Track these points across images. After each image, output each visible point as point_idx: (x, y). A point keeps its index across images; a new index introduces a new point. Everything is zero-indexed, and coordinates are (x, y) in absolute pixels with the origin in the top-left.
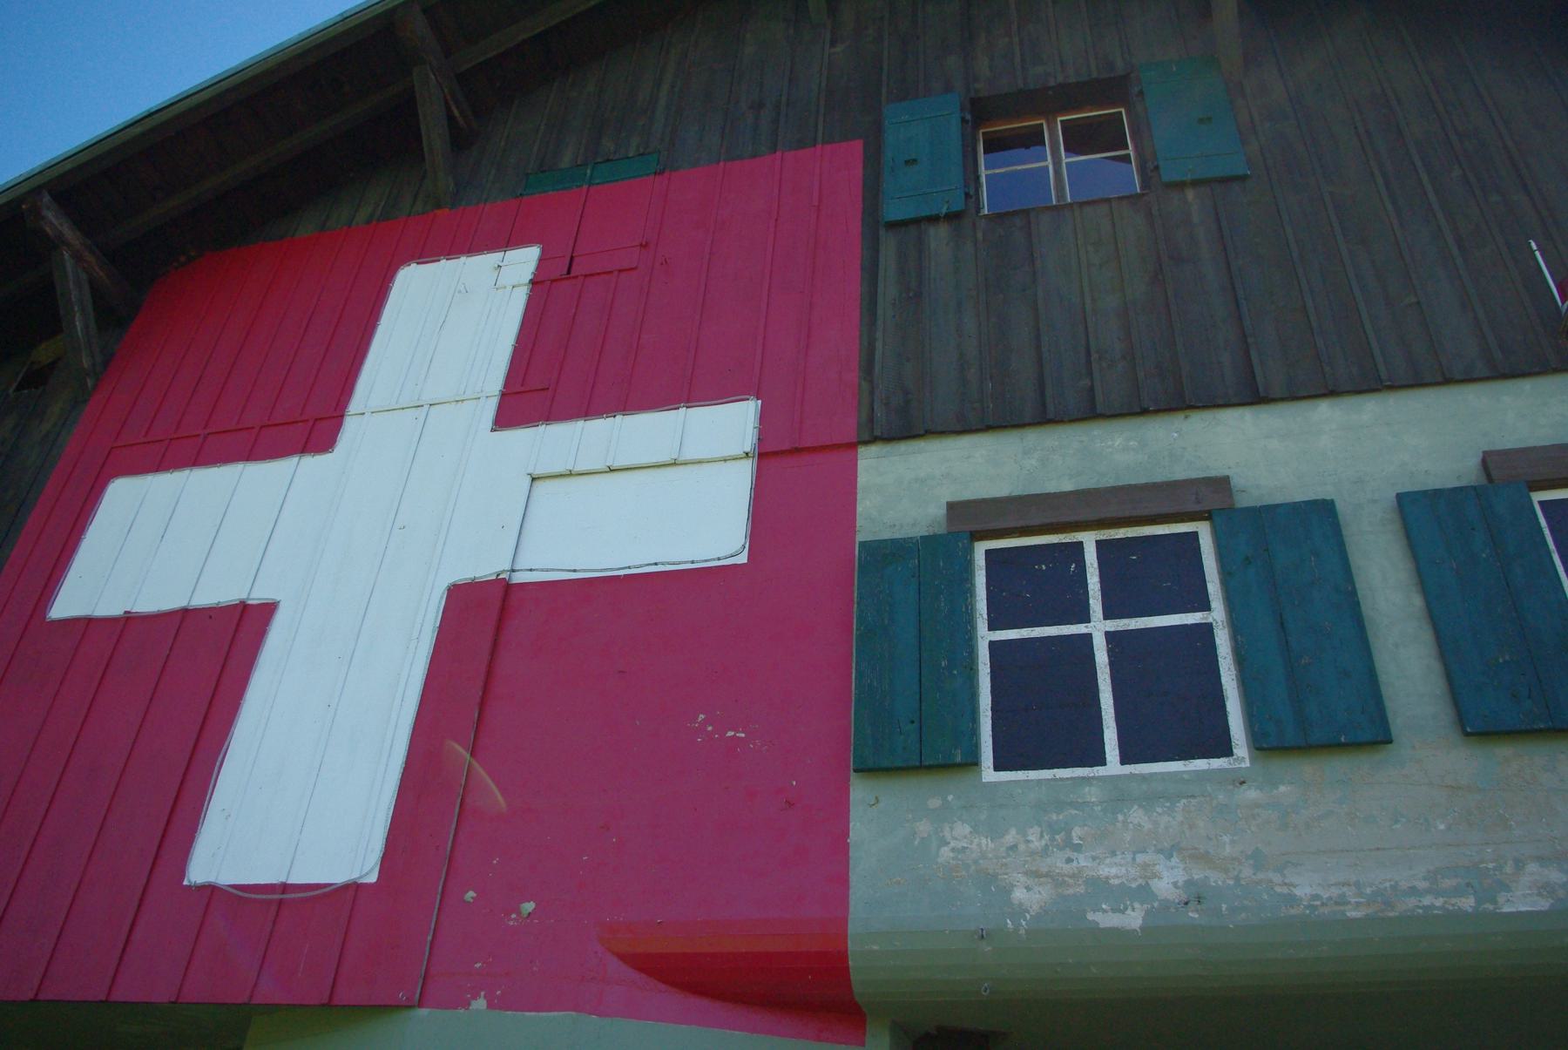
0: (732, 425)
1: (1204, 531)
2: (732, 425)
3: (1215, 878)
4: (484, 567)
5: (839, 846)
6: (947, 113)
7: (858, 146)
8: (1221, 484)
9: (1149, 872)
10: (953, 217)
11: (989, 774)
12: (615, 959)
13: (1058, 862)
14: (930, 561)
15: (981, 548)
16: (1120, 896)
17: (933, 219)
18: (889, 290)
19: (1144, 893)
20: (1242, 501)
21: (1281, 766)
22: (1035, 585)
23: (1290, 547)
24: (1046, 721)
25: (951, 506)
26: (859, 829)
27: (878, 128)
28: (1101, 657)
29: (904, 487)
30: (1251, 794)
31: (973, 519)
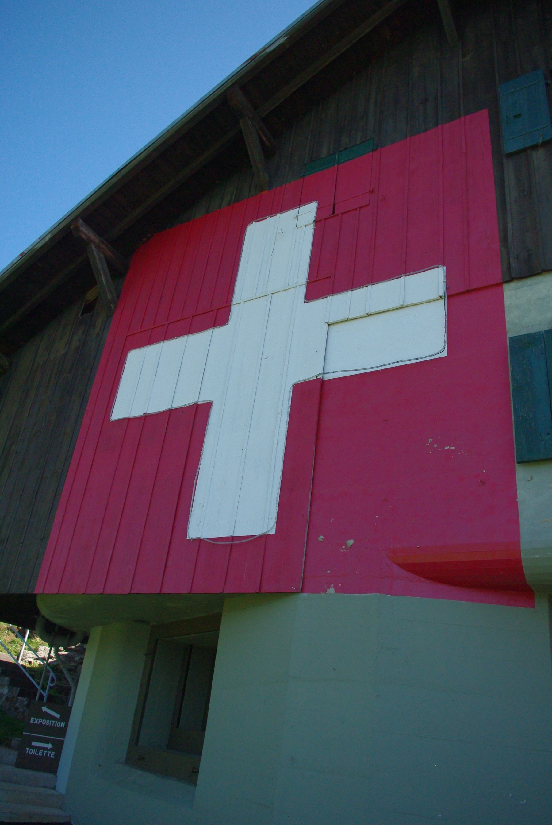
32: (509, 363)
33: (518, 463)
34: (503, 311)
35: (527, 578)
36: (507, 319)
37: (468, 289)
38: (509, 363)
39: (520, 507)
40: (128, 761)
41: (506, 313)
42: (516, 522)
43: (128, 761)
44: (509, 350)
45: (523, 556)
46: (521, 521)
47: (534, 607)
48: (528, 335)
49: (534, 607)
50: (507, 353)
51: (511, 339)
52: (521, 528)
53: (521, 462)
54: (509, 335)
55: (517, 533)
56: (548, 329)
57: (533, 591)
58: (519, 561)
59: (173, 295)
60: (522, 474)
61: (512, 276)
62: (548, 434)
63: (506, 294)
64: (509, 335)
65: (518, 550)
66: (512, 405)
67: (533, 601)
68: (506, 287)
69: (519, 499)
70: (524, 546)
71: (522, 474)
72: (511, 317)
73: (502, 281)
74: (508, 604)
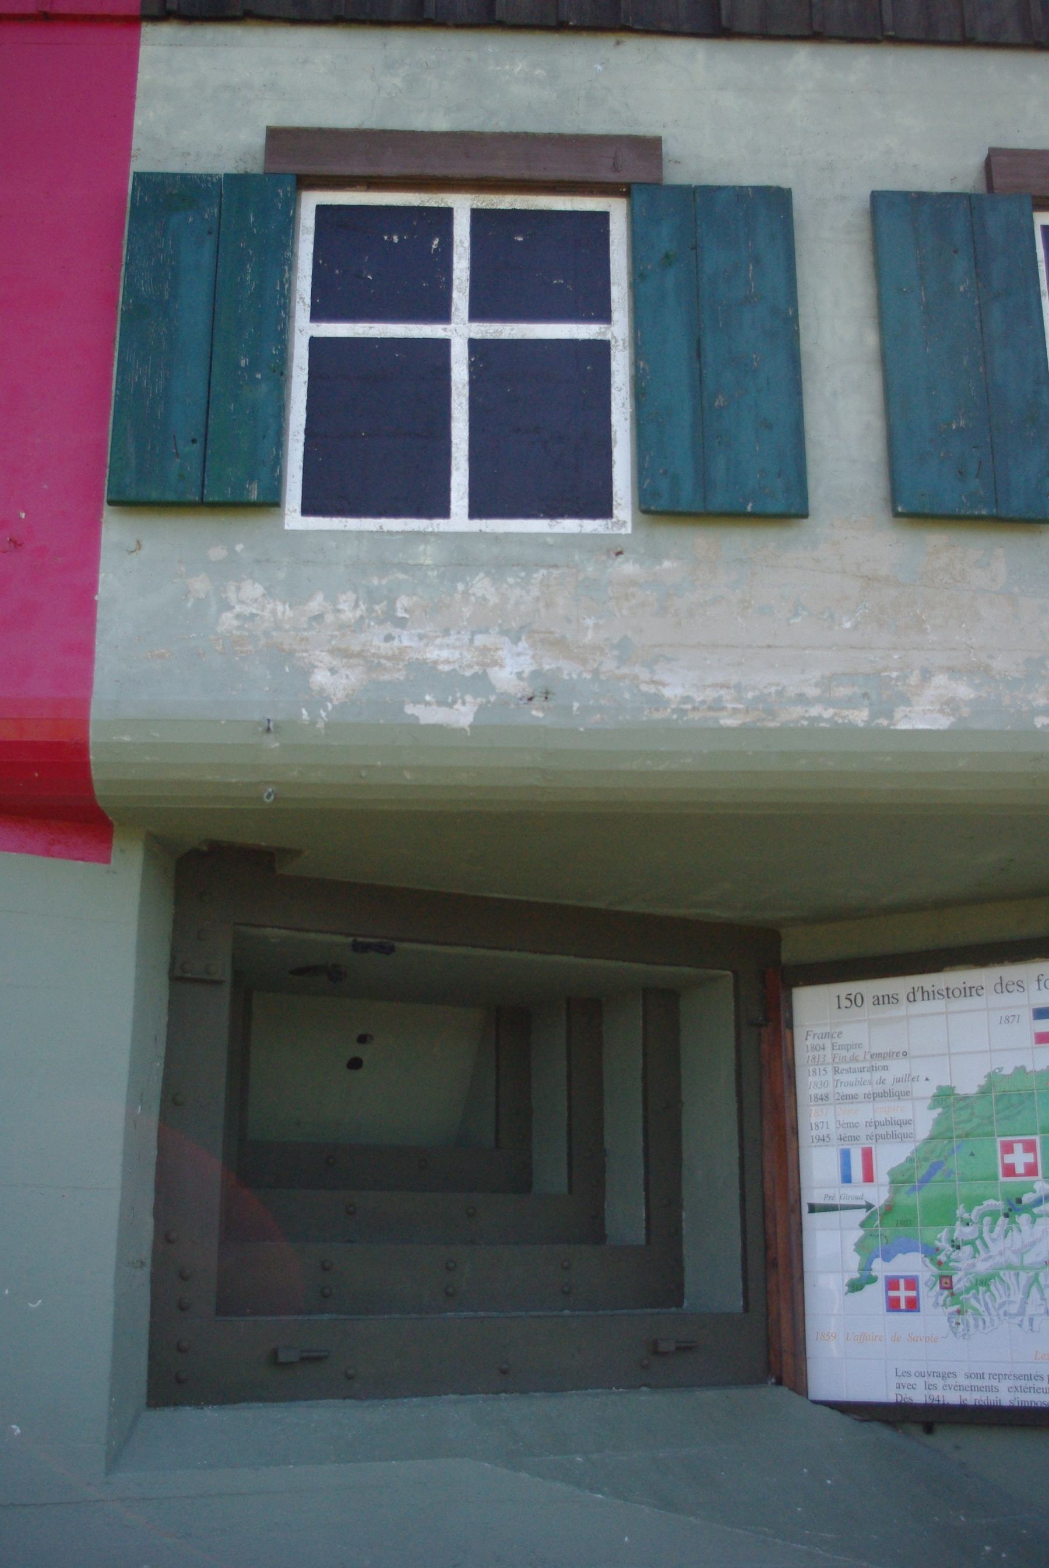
3: (570, 670)
8: (649, 147)
9: (488, 658)
11: (293, 517)
13: (375, 640)
15: (310, 201)
16: (448, 686)
19: (480, 683)
20: (675, 175)
23: (724, 243)
24: (376, 456)
25: (276, 136)
30: (627, 568)
31: (302, 155)
32: (125, 242)
33: (111, 503)
34: (132, 97)
35: (99, 790)
36: (138, 122)
37: (47, 9)
38: (125, 242)
39: (101, 614)
40: (888, 1310)
41: (139, 103)
42: (85, 650)
43: (888, 1310)
44: (129, 205)
45: (94, 737)
46: (101, 648)
47: (107, 861)
48: (185, 177)
49: (107, 861)
50: (123, 212)
51: (138, 176)
52: (97, 666)
53: (124, 503)
54: (136, 166)
55: (84, 677)
56: (234, 172)
57: (110, 825)
58: (81, 749)
59: (933, 1056)
60: (116, 530)
61: (169, 6)
62: (194, 441)
63: (146, 52)
64: (136, 166)
65: (83, 723)
66: (116, 354)
67: (110, 848)
68: (148, 31)
69: (102, 594)
70: (97, 713)
71: (116, 530)
72: (147, 117)
73: (138, 13)
74: (47, 853)
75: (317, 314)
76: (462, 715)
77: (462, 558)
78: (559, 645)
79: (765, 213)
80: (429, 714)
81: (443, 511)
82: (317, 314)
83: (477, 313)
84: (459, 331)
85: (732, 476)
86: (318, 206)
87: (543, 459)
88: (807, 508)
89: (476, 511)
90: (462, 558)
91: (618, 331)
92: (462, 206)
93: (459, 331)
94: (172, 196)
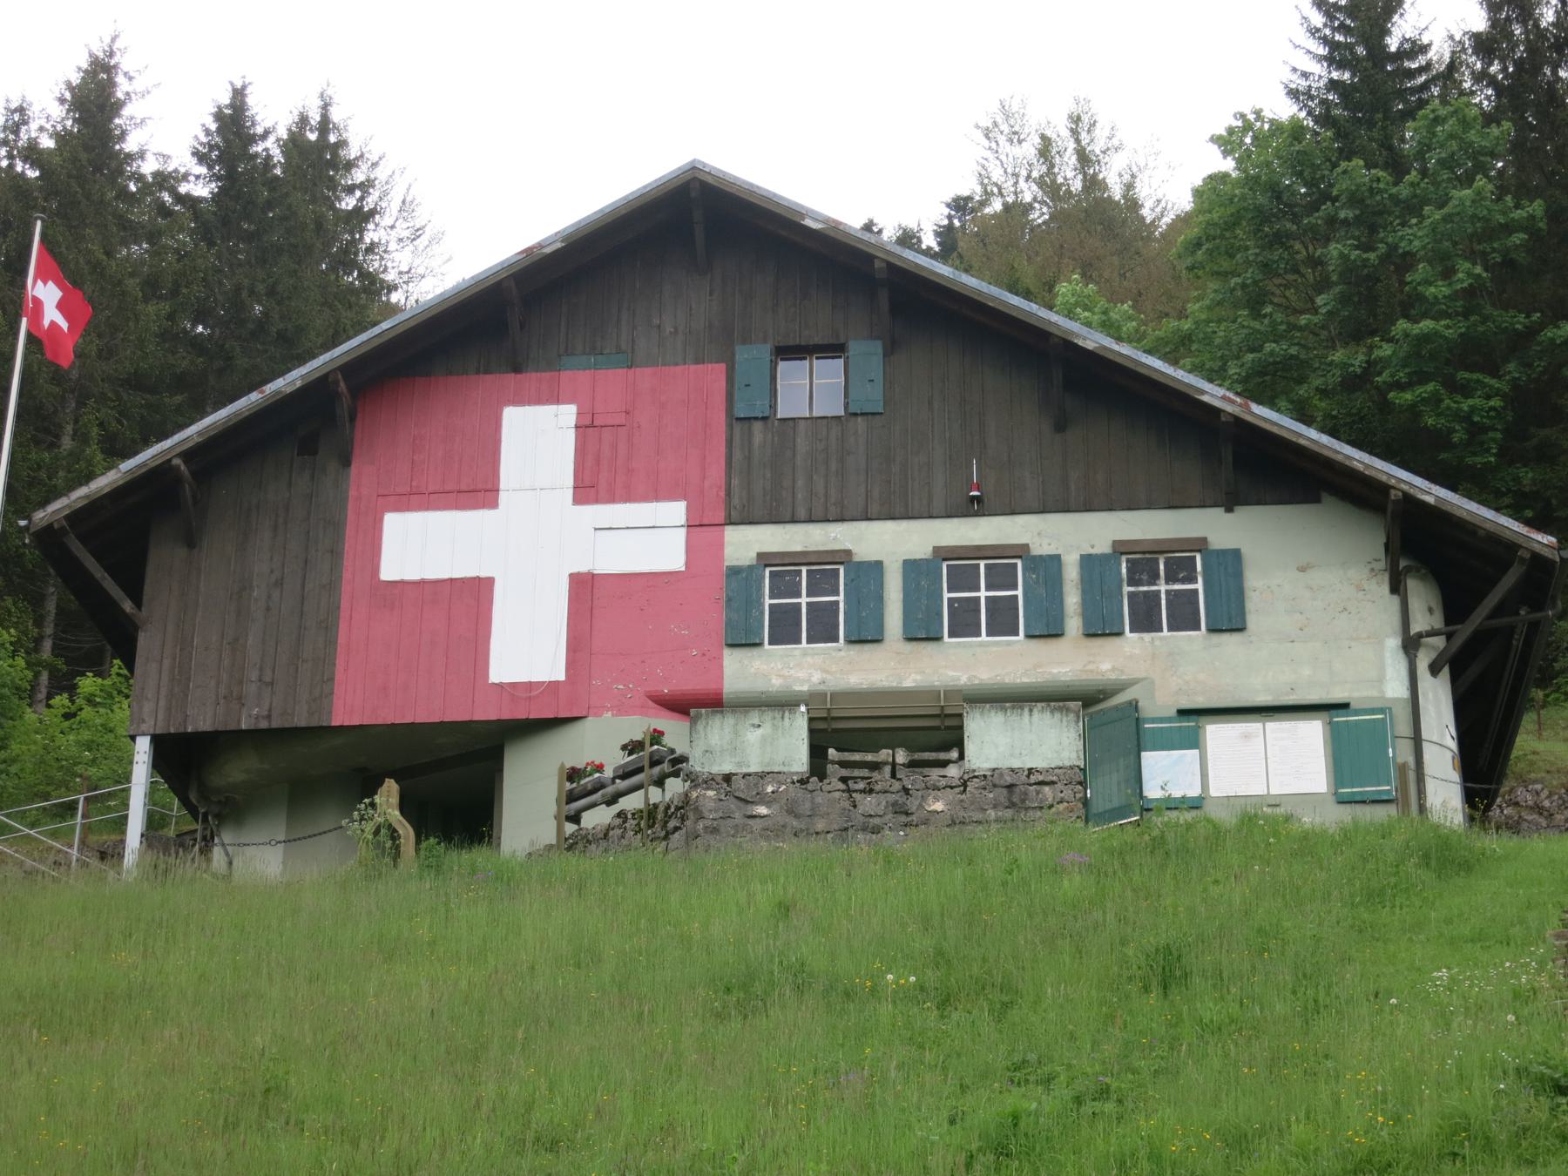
0: (675, 511)
1: (1019, 563)
2: (675, 511)
3: (829, 677)
4: (583, 569)
5: (721, 666)
6: (764, 351)
7: (723, 366)
8: (848, 553)
9: (811, 675)
10: (764, 419)
11: (984, 637)
12: (1137, 675)
13: (785, 672)
14: (742, 577)
15: (767, 571)
16: (803, 682)
17: (756, 418)
18: (738, 455)
19: (809, 680)
20: (856, 559)
21: (852, 647)
22: (784, 585)
23: (1047, 569)
24: (785, 630)
25: (1115, 542)
26: (726, 662)
27: (733, 354)
28: (1163, 596)
29: (745, 543)
30: (843, 653)
31: (765, 559)
58: (721, 694)
75: (949, 591)
76: (805, 688)
77: (981, 644)
78: (827, 672)
79: (876, 569)
80: (797, 688)
81: (979, 635)
82: (949, 591)
83: (808, 595)
84: (1162, 588)
85: (867, 635)
86: (571, 575)
87: (823, 630)
88: (1244, 621)
89: (988, 634)
90: (805, 653)
91: (841, 598)
92: (982, 564)
93: (804, 600)
94: (734, 571)
